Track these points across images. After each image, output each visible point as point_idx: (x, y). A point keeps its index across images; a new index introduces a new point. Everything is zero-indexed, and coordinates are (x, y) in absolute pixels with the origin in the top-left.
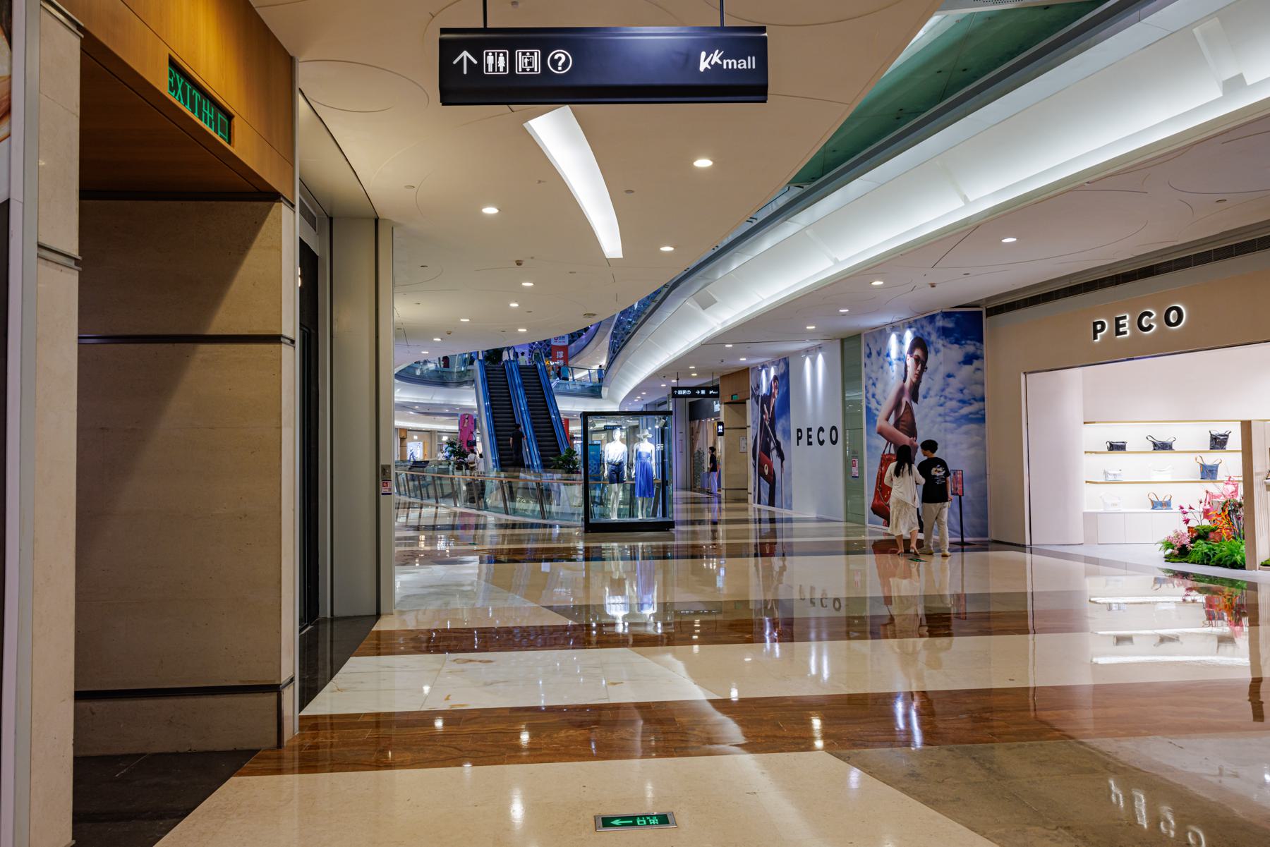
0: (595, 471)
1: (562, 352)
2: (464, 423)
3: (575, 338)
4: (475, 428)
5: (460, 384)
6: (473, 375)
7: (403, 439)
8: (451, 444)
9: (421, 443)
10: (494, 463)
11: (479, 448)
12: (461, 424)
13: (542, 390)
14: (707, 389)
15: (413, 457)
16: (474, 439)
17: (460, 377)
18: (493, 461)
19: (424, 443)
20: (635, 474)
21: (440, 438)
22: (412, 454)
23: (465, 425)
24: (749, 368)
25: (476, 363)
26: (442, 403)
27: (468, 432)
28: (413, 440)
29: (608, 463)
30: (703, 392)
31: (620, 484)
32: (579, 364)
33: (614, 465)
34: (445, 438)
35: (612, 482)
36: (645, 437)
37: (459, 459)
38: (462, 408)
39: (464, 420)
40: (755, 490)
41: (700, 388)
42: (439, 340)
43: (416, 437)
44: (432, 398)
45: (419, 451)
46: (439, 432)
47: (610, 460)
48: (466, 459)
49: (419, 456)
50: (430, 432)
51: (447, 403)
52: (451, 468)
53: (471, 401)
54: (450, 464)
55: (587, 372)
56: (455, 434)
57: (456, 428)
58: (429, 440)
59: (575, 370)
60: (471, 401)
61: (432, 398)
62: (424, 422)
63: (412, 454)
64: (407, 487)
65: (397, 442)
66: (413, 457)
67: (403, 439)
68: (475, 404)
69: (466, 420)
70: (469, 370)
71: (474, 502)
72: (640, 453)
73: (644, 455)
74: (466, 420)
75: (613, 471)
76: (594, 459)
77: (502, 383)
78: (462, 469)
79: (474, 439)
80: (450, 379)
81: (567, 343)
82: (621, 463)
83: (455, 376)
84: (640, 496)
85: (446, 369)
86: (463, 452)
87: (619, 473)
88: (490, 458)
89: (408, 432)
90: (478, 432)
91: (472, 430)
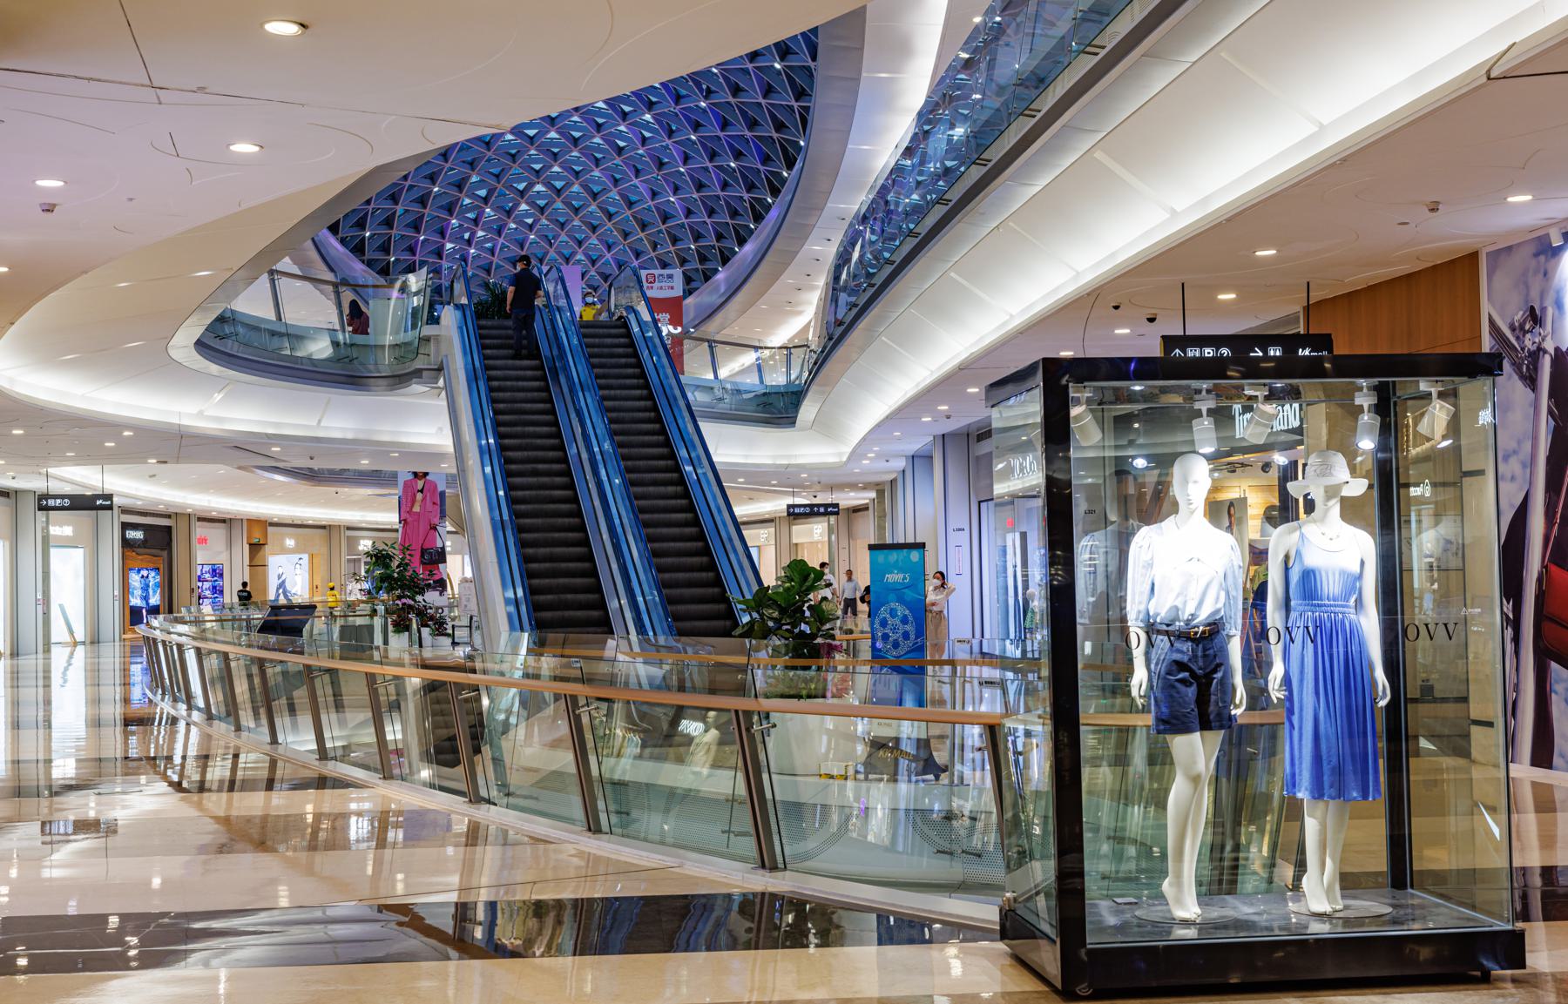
0: (905, 646)
1: (668, 316)
2: (413, 501)
3: (693, 285)
4: (443, 515)
5: (399, 380)
6: (437, 351)
7: (256, 548)
8: (379, 558)
9: (306, 557)
10: (512, 609)
11: (457, 568)
12: (404, 506)
13: (651, 397)
14: (1290, 342)
15: (285, 593)
16: (439, 544)
17: (400, 359)
18: (507, 601)
19: (312, 557)
20: (1287, 681)
21: (352, 543)
22: (282, 585)
23: (417, 509)
24: (1473, 257)
25: (449, 316)
26: (350, 436)
27: (423, 527)
28: (284, 551)
29: (1151, 629)
30: (1275, 352)
31: (1207, 734)
32: (733, 332)
33: (1183, 636)
34: (365, 545)
35: (1172, 723)
36: (1331, 492)
37: (399, 598)
38: (410, 453)
39: (414, 496)
40: (1512, 709)
41: (1264, 341)
42: (291, 29)
43: (290, 543)
44: (320, 421)
45: (299, 579)
46: (349, 528)
47: (1161, 609)
48: (419, 598)
49: (300, 591)
50: (327, 529)
51: (361, 436)
52: (378, 622)
53: (433, 430)
54: (374, 612)
55: (749, 358)
56: (393, 535)
57: (391, 518)
58: (324, 550)
59: (719, 349)
60: (433, 430)
61: (320, 421)
62: (313, 503)
63: (282, 585)
64: (257, 680)
65: (901, 659)
66: (285, 593)
67: (256, 548)
68: (445, 442)
69: (419, 496)
70: (427, 339)
71: (454, 763)
72: (1309, 575)
73: (1331, 586)
74: (419, 496)
75: (1180, 666)
76: (901, 600)
77: (529, 373)
78: (407, 628)
79: (439, 544)
80: (371, 367)
81: (678, 291)
82: (1215, 628)
83: (387, 358)
84: (1318, 793)
85: (360, 339)
86: (412, 579)
87: (1209, 677)
88: (500, 598)
89: (270, 529)
90: (450, 528)
91: (436, 520)
